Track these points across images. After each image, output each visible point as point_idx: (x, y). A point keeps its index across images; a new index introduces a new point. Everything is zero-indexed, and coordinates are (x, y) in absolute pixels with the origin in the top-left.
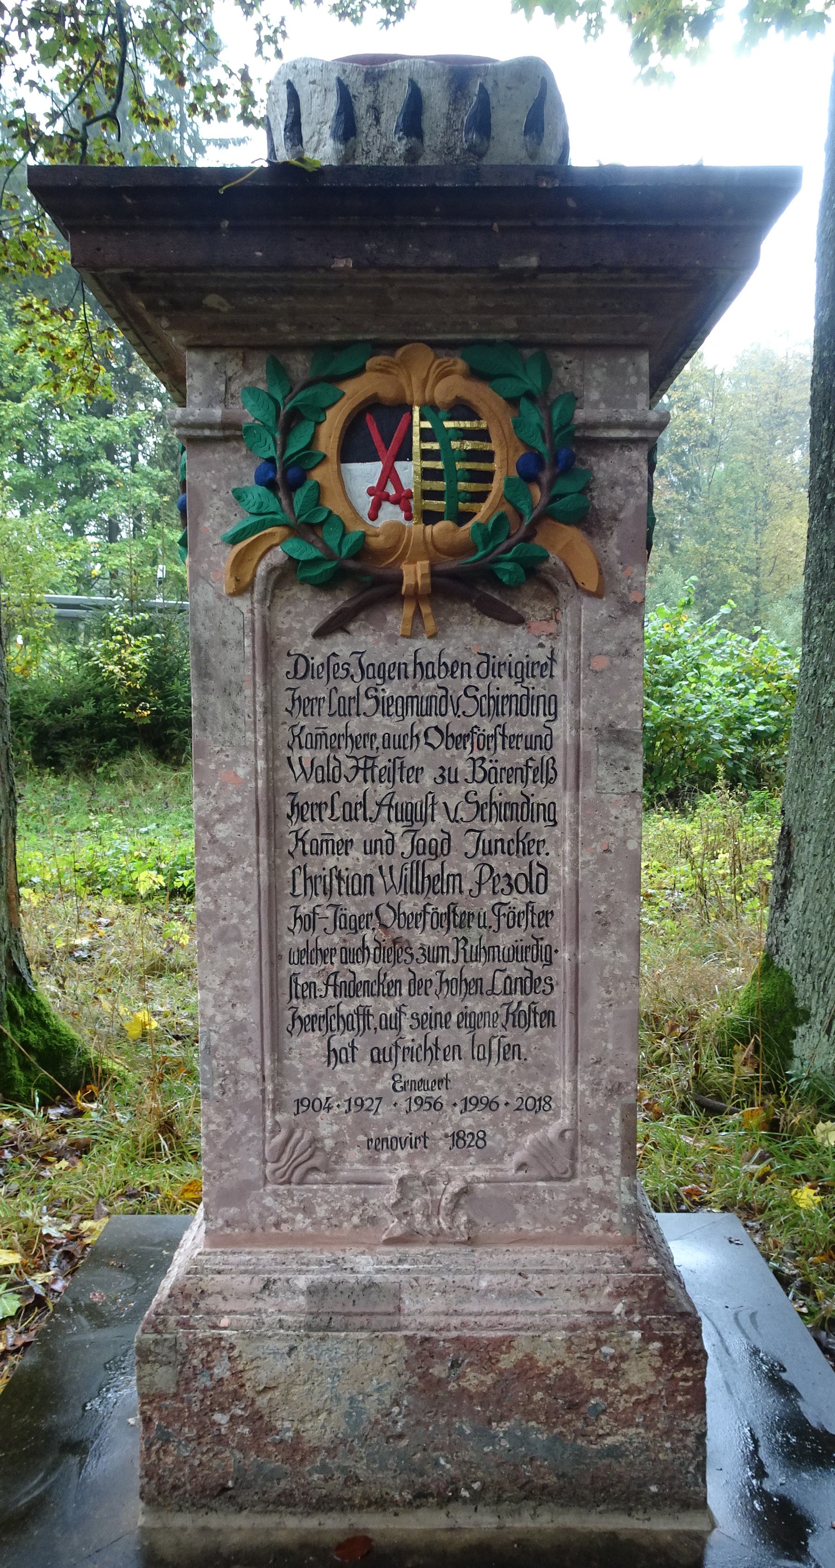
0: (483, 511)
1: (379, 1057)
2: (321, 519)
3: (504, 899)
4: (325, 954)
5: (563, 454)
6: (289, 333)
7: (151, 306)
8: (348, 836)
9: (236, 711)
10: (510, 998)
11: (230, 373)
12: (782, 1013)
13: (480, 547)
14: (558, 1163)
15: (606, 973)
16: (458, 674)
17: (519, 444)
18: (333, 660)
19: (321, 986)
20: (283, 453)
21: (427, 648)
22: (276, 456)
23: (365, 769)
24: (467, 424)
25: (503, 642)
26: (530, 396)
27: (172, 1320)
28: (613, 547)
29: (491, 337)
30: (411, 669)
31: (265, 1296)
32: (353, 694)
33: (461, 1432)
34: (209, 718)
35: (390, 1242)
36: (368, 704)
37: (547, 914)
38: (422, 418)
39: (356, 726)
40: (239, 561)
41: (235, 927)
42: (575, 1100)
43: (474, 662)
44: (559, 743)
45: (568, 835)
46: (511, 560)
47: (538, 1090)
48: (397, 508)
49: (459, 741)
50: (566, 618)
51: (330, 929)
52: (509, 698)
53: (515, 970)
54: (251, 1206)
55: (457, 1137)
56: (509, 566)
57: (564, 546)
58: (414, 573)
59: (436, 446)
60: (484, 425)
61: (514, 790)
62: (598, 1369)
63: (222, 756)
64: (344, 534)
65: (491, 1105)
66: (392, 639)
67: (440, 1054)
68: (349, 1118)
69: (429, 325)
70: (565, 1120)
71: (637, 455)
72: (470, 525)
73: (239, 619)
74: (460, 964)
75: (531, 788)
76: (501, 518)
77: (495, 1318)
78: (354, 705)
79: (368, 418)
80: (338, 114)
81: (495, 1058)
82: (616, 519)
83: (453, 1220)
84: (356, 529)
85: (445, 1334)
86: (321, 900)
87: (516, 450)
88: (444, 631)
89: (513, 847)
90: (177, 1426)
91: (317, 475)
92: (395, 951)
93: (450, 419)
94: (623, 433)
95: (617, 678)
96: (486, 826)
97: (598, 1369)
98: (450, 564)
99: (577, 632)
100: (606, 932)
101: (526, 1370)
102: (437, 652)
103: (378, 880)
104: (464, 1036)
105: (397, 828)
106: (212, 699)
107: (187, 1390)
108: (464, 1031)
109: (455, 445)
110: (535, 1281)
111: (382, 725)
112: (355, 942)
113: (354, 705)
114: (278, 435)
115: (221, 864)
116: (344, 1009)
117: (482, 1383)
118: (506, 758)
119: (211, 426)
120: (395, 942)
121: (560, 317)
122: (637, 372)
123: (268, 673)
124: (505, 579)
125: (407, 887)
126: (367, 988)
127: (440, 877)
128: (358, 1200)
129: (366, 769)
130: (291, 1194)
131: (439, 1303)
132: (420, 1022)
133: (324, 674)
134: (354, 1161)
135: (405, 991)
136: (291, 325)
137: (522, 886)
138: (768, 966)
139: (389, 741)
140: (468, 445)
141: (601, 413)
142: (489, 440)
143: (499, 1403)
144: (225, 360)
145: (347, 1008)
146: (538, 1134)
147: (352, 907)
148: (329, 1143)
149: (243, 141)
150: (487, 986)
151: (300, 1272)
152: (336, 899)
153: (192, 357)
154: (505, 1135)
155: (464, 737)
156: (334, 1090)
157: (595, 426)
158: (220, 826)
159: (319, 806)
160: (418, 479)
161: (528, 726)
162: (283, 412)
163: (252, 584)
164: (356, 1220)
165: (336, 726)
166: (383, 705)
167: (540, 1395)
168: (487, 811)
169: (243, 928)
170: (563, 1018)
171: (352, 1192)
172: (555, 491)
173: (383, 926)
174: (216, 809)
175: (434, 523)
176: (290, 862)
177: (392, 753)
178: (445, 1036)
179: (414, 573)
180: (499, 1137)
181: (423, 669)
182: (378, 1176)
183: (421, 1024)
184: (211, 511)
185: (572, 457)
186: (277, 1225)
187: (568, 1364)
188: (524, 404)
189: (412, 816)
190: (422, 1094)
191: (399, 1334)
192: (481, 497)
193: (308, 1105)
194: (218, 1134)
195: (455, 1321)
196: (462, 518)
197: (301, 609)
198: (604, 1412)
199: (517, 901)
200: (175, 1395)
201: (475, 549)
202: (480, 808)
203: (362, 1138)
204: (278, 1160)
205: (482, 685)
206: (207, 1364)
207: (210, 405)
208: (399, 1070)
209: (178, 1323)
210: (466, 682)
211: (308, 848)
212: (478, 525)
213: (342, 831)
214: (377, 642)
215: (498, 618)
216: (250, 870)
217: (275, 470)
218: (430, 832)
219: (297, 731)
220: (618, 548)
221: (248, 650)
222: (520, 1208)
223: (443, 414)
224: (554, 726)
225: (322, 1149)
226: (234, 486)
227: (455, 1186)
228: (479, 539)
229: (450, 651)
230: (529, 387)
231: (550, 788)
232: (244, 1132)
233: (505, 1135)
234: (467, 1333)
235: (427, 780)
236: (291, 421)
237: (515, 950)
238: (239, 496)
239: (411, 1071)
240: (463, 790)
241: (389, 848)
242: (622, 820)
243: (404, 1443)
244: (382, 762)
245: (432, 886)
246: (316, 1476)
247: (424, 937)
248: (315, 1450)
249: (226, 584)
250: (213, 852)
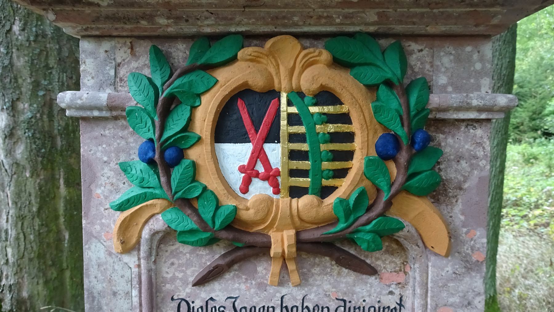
0: (344, 187)
2: (196, 194)
5: (419, 137)
6: (167, 26)
11: (119, 60)
13: (342, 219)
17: (378, 126)
18: (211, 304)
20: (161, 135)
22: (155, 138)
25: (358, 289)
26: (388, 83)
28: (458, 212)
29: (351, 29)
40: (125, 227)
46: (370, 232)
48: (266, 184)
50: (415, 272)
56: (368, 237)
57: (418, 213)
64: (218, 207)
66: (262, 286)
69: (296, 19)
73: (128, 274)
76: (362, 194)
79: (239, 102)
82: (461, 189)
84: (229, 203)
87: (376, 132)
88: (307, 280)
91: (194, 154)
93: (315, 105)
94: (472, 115)
99: (425, 286)
102: (300, 297)
114: (157, 119)
119: (100, 109)
121: (418, 10)
122: (482, 60)
136: (168, 18)
140: (331, 128)
141: (454, 98)
142: (350, 123)
144: (114, 48)
157: (446, 110)
160: (286, 159)
162: (161, 98)
163: (138, 243)
172: (411, 171)
175: (299, 196)
184: (103, 180)
185: (429, 139)
188: (383, 90)
192: (342, 173)
197: (183, 261)
214: (248, 289)
215: (355, 270)
217: (154, 151)
220: (463, 214)
221: (136, 300)
228: (341, 215)
229: (312, 296)
230: (389, 75)
236: (167, 107)
249: (115, 245)
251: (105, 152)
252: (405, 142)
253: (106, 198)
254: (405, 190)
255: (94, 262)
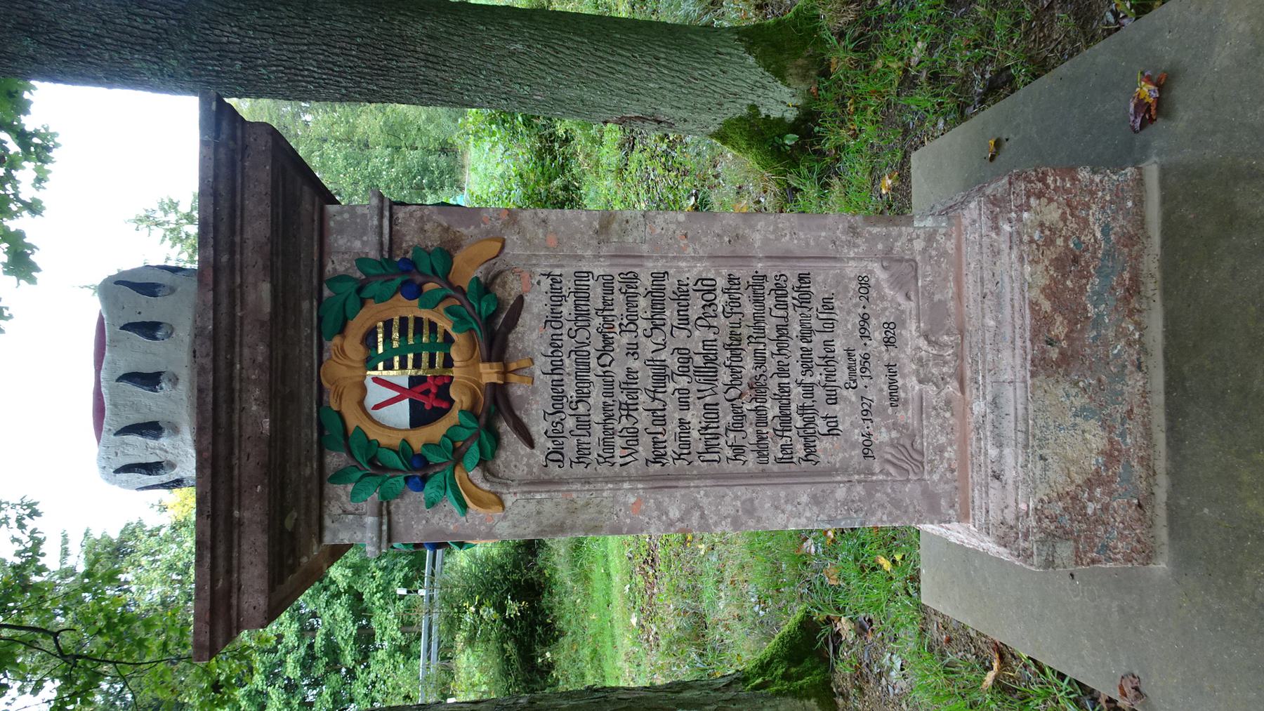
0: (444, 324)
1: (833, 399)
3: (720, 309)
4: (761, 438)
7: (292, 570)
8: (676, 422)
9: (588, 504)
10: (790, 305)
12: (752, 125)
14: (904, 271)
15: (772, 237)
16: (559, 343)
19: (784, 441)
21: (541, 364)
22: (404, 475)
23: (628, 410)
24: (380, 336)
25: (536, 310)
26: (359, 290)
27: (1022, 544)
30: (556, 377)
31: (1004, 478)
32: (574, 419)
33: (1095, 339)
34: (592, 524)
35: (962, 390)
36: (582, 408)
37: (731, 279)
38: (376, 369)
39: (597, 417)
40: (479, 502)
41: (743, 503)
42: (861, 259)
43: (552, 331)
44: (608, 271)
45: (675, 263)
47: (854, 285)
49: (607, 342)
51: (743, 434)
52: (576, 306)
53: (770, 302)
54: (941, 488)
55: (888, 343)
56: (484, 305)
58: (489, 374)
59: (397, 359)
60: (381, 324)
61: (643, 303)
62: (1049, 242)
63: (621, 514)
64: (461, 426)
65: (865, 319)
66: (534, 392)
67: (830, 355)
68: (876, 420)
70: (876, 267)
71: (401, 213)
72: (454, 334)
73: (522, 502)
74: (767, 341)
75: (641, 290)
76: (449, 311)
77: (1017, 315)
78: (582, 418)
80: (142, 435)
81: (832, 316)
83: (946, 345)
85: (1028, 350)
86: (722, 441)
89: (684, 303)
90: (1097, 540)
92: (757, 387)
93: (376, 348)
94: (386, 223)
95: (562, 228)
96: (669, 323)
97: (1049, 242)
98: (481, 348)
100: (744, 237)
101: (1051, 292)
103: (708, 400)
104: (818, 338)
105: (671, 386)
106: (579, 522)
107: (1072, 532)
108: (814, 338)
109: (396, 345)
110: (989, 286)
111: (596, 398)
112: (752, 416)
113: (582, 418)
115: (698, 513)
116: (800, 424)
117: (1062, 323)
118: (619, 308)
119: (381, 524)
120: (751, 388)
123: (561, 482)
124: (493, 308)
125: (712, 379)
126: (784, 408)
127: (705, 356)
128: (933, 413)
129: (628, 410)
130: (931, 461)
131: (1006, 354)
132: (807, 369)
133: (560, 440)
134: (907, 415)
135: (786, 380)
137: (711, 297)
138: (722, 137)
139: (608, 393)
140: (396, 335)
141: (372, 238)
143: (1075, 313)
145: (799, 423)
146: (885, 285)
147: (727, 418)
148: (894, 434)
149: (65, 536)
150: (782, 322)
151: (986, 454)
152: (722, 430)
153: (328, 539)
154: (885, 309)
155: (605, 338)
156: (856, 431)
157: (381, 244)
158: (671, 515)
159: (655, 443)
161: (597, 293)
162: (371, 471)
163: (495, 493)
164: (948, 415)
165: (598, 431)
166: (582, 397)
167: (1068, 283)
168: (658, 322)
169: (744, 498)
170: (804, 266)
171: (928, 417)
172: (429, 273)
173: (740, 396)
174: (659, 518)
176: (696, 463)
177: (617, 390)
178: (818, 351)
179: (489, 374)
180: (887, 313)
181: (556, 368)
182: (916, 399)
183: (809, 369)
184: (442, 524)
186: (953, 471)
187: (1047, 263)
189: (661, 376)
190: (858, 368)
191: (1029, 382)
192: (433, 326)
193: (867, 451)
194: (890, 514)
195: (1019, 343)
196: (448, 340)
198: (1079, 238)
199: (721, 300)
200: (1076, 541)
201: (471, 330)
202: (656, 327)
203: (890, 410)
204: (907, 471)
205: (567, 325)
206: (1053, 519)
207: (363, 526)
208: (842, 384)
209: (1025, 540)
210: (565, 337)
211: (685, 451)
212: (454, 328)
213: (673, 427)
214: (537, 402)
215: (519, 314)
216: (702, 493)
218: (673, 363)
219: (601, 460)
221: (544, 496)
222: (937, 297)
223: (372, 353)
224: (596, 273)
225: (898, 439)
226: (423, 507)
227: (923, 343)
228: (466, 327)
230: (353, 290)
231: (641, 276)
232: (888, 495)
233: (885, 309)
234: (1028, 335)
235: (636, 365)
237: (756, 301)
238: (432, 504)
239: (842, 376)
240: (643, 339)
241: (684, 392)
242: (664, 225)
243: (1103, 378)
244: (623, 398)
245: (712, 361)
246: (1128, 441)
247: (748, 366)
248: (1111, 441)
249: (496, 512)
250: (689, 520)
251: (418, 522)
252: (406, 277)
253: (457, 521)
254: (445, 278)
255: (511, 531)
